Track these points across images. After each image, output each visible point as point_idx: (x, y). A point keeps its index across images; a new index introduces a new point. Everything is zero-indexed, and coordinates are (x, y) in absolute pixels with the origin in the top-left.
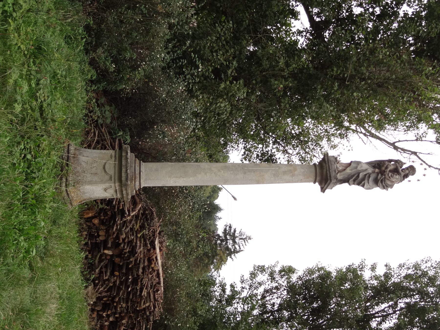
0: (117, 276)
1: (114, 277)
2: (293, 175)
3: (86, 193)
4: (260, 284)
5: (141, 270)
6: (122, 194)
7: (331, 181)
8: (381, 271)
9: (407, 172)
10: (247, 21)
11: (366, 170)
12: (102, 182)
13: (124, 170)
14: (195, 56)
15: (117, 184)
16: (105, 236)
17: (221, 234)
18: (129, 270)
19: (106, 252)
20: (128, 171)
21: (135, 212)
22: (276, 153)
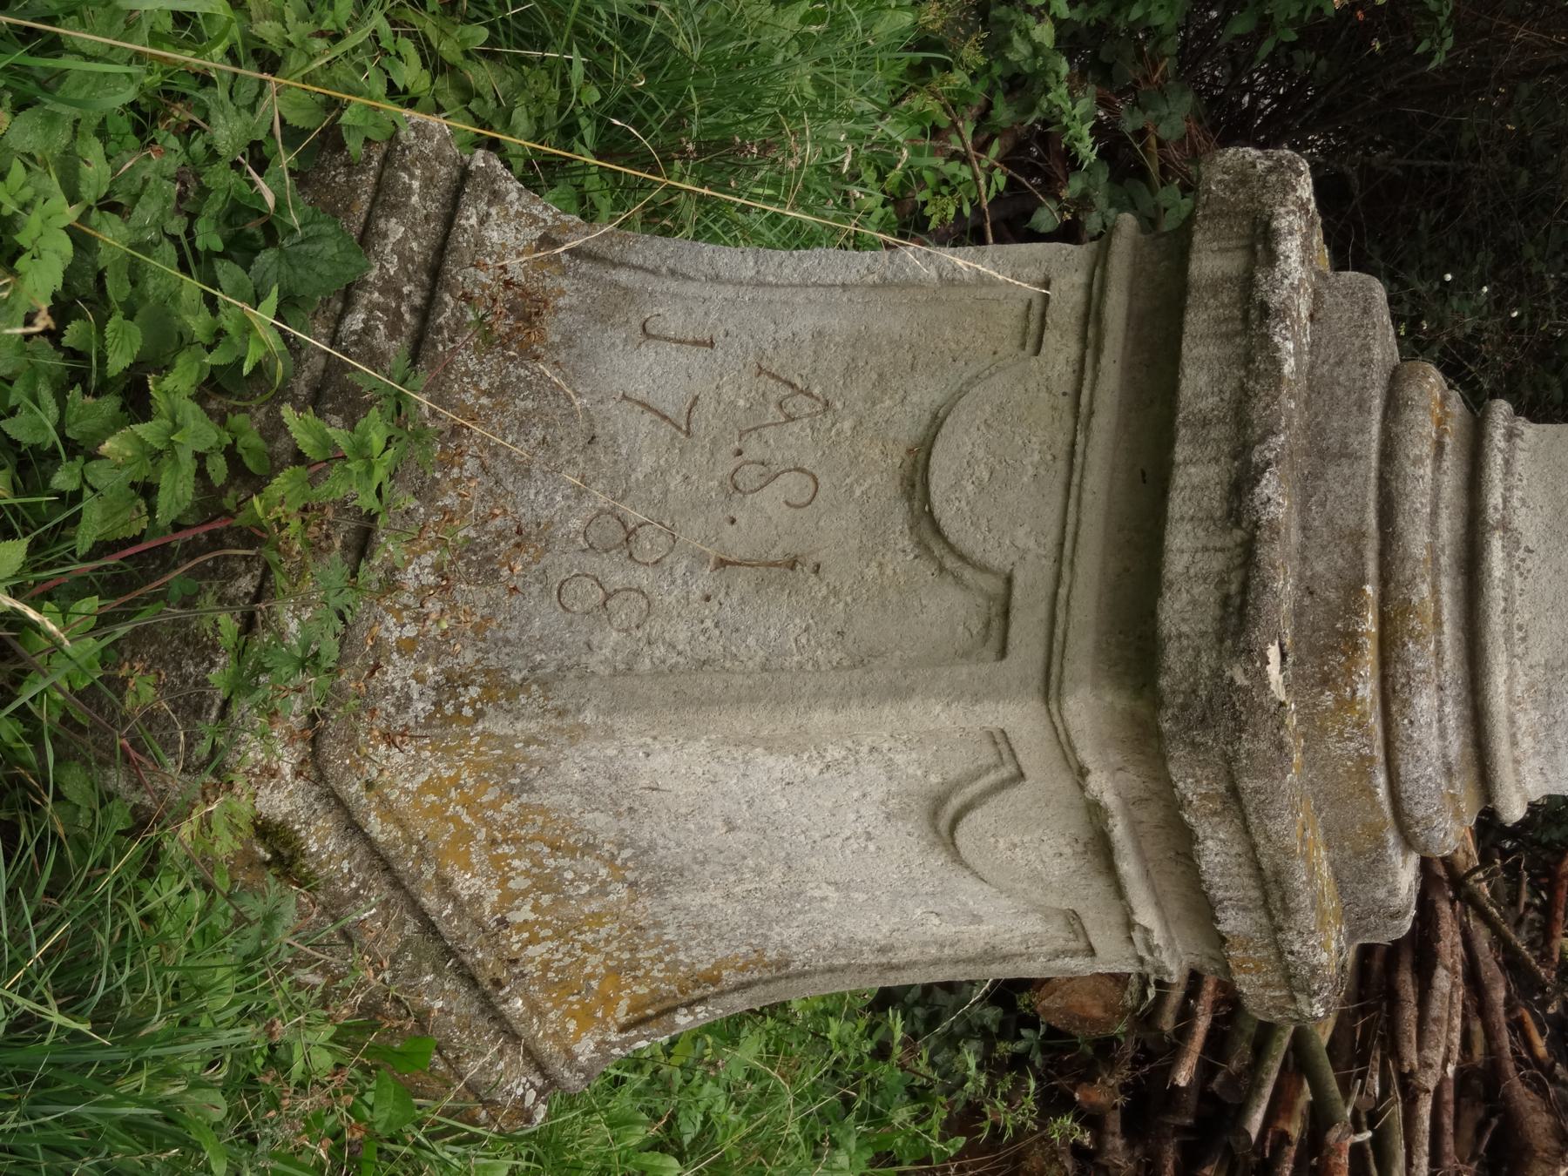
6: (1200, 907)
12: (871, 672)
13: (1196, 476)
15: (1088, 709)
20: (1269, 486)
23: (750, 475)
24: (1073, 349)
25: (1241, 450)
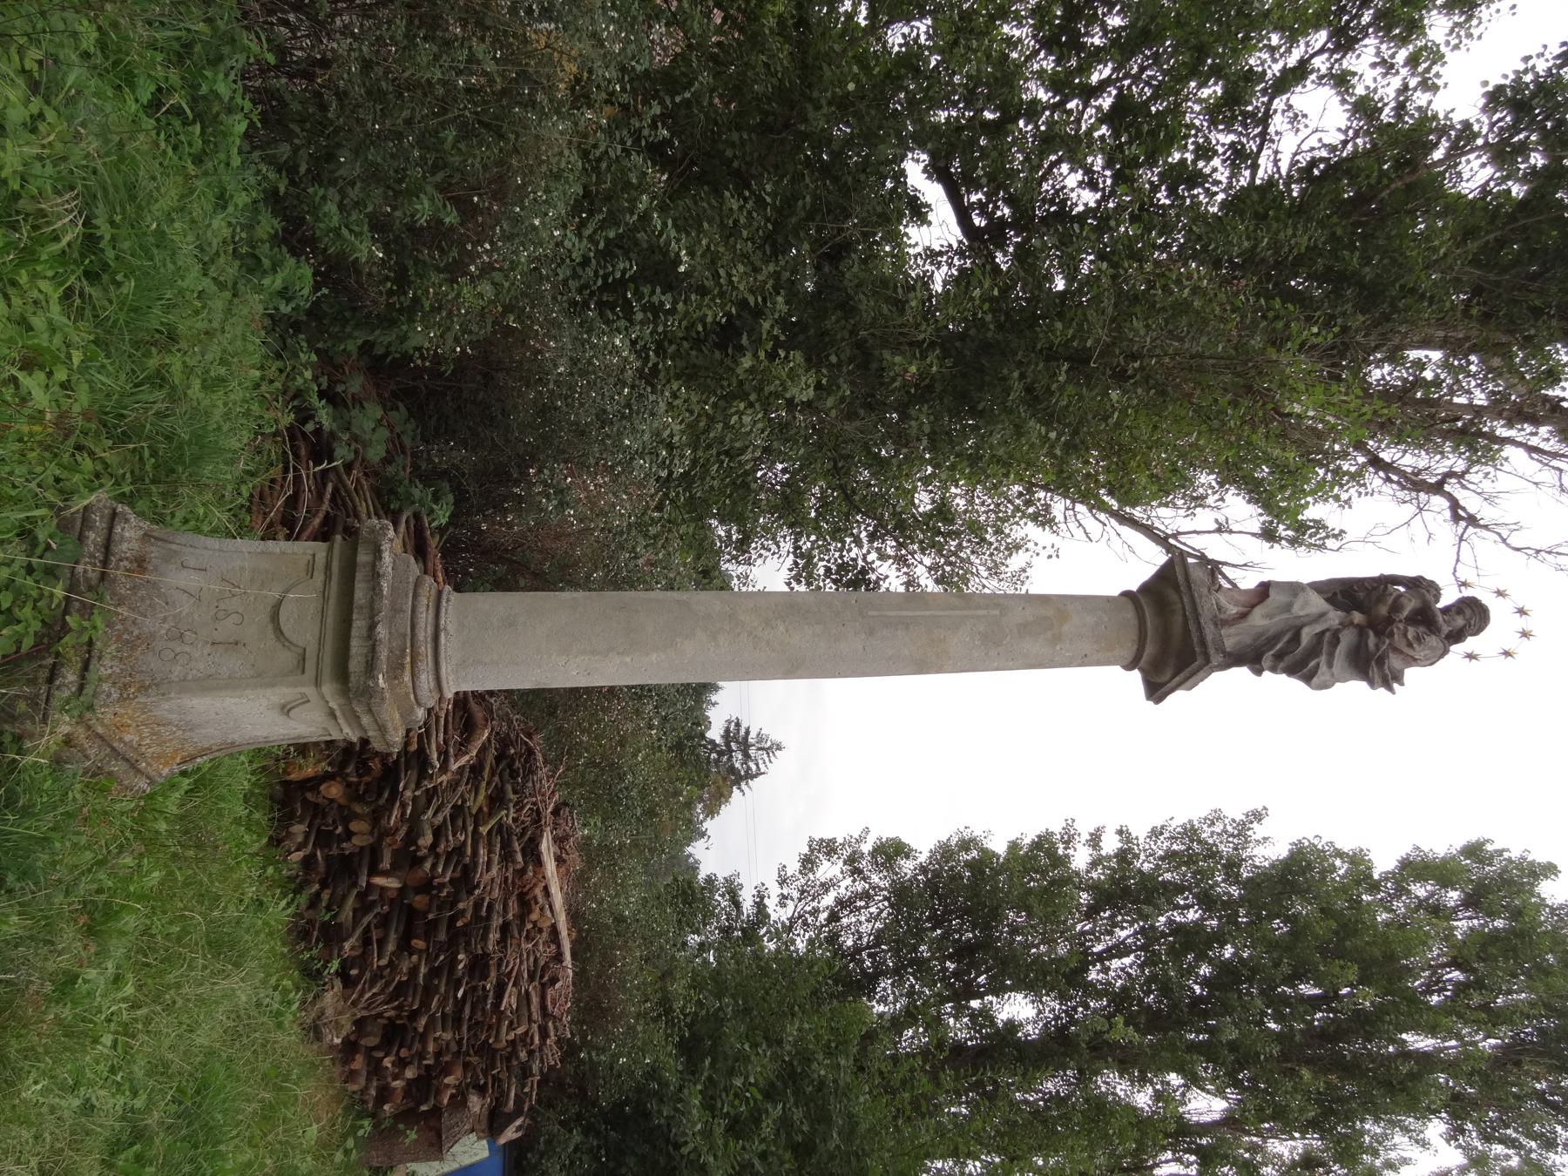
0: (420, 952)
1: (411, 955)
2: (1057, 639)
3: (199, 726)
4: (826, 887)
5: (494, 936)
7: (1208, 661)
8: (1111, 844)
9: (1460, 621)
10: (808, 199)
11: (1322, 615)
12: (261, 679)
13: (359, 624)
14: (665, 224)
15: (328, 689)
16: (371, 833)
17: (719, 740)
18: (457, 938)
19: (379, 881)
20: (380, 628)
21: (467, 758)
22: (878, 563)
23: (221, 615)
24: (322, 578)
25: (372, 617)
